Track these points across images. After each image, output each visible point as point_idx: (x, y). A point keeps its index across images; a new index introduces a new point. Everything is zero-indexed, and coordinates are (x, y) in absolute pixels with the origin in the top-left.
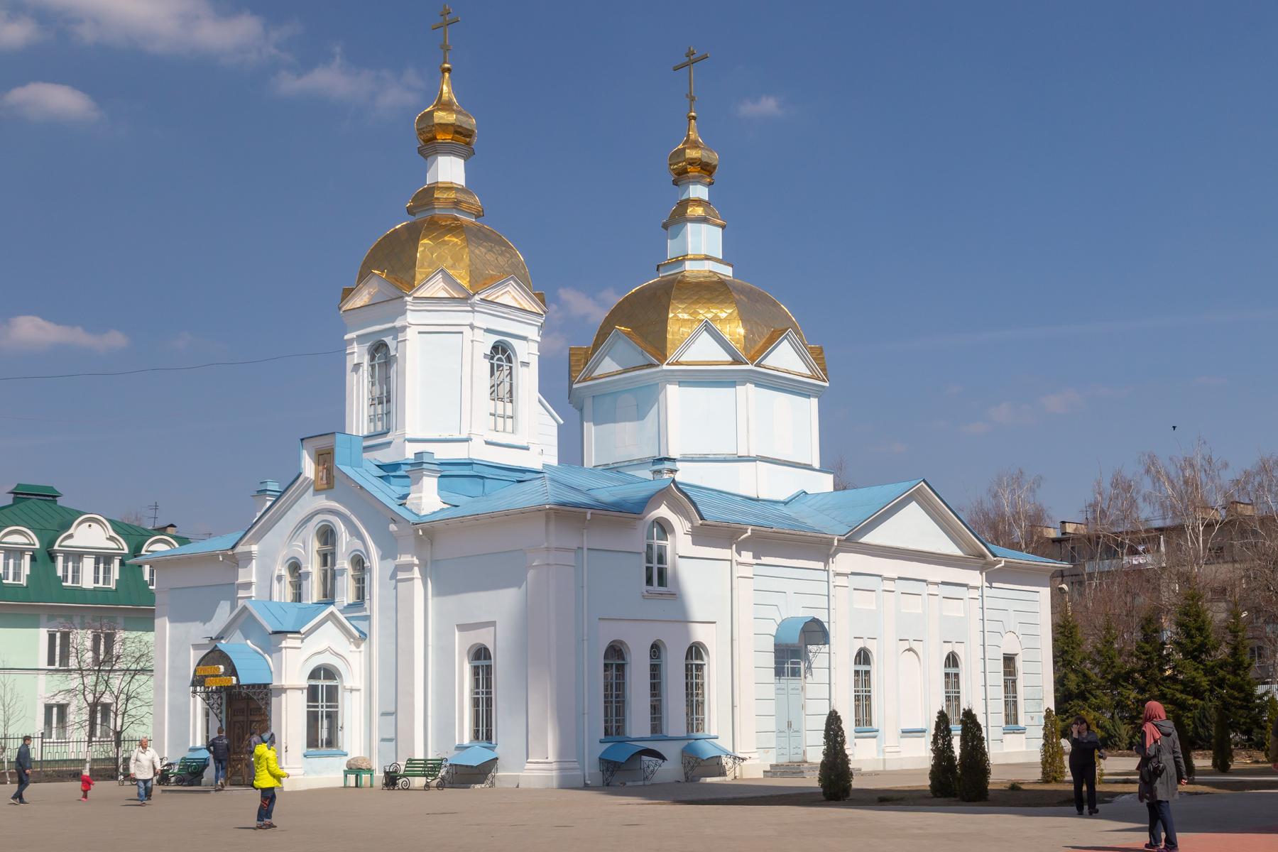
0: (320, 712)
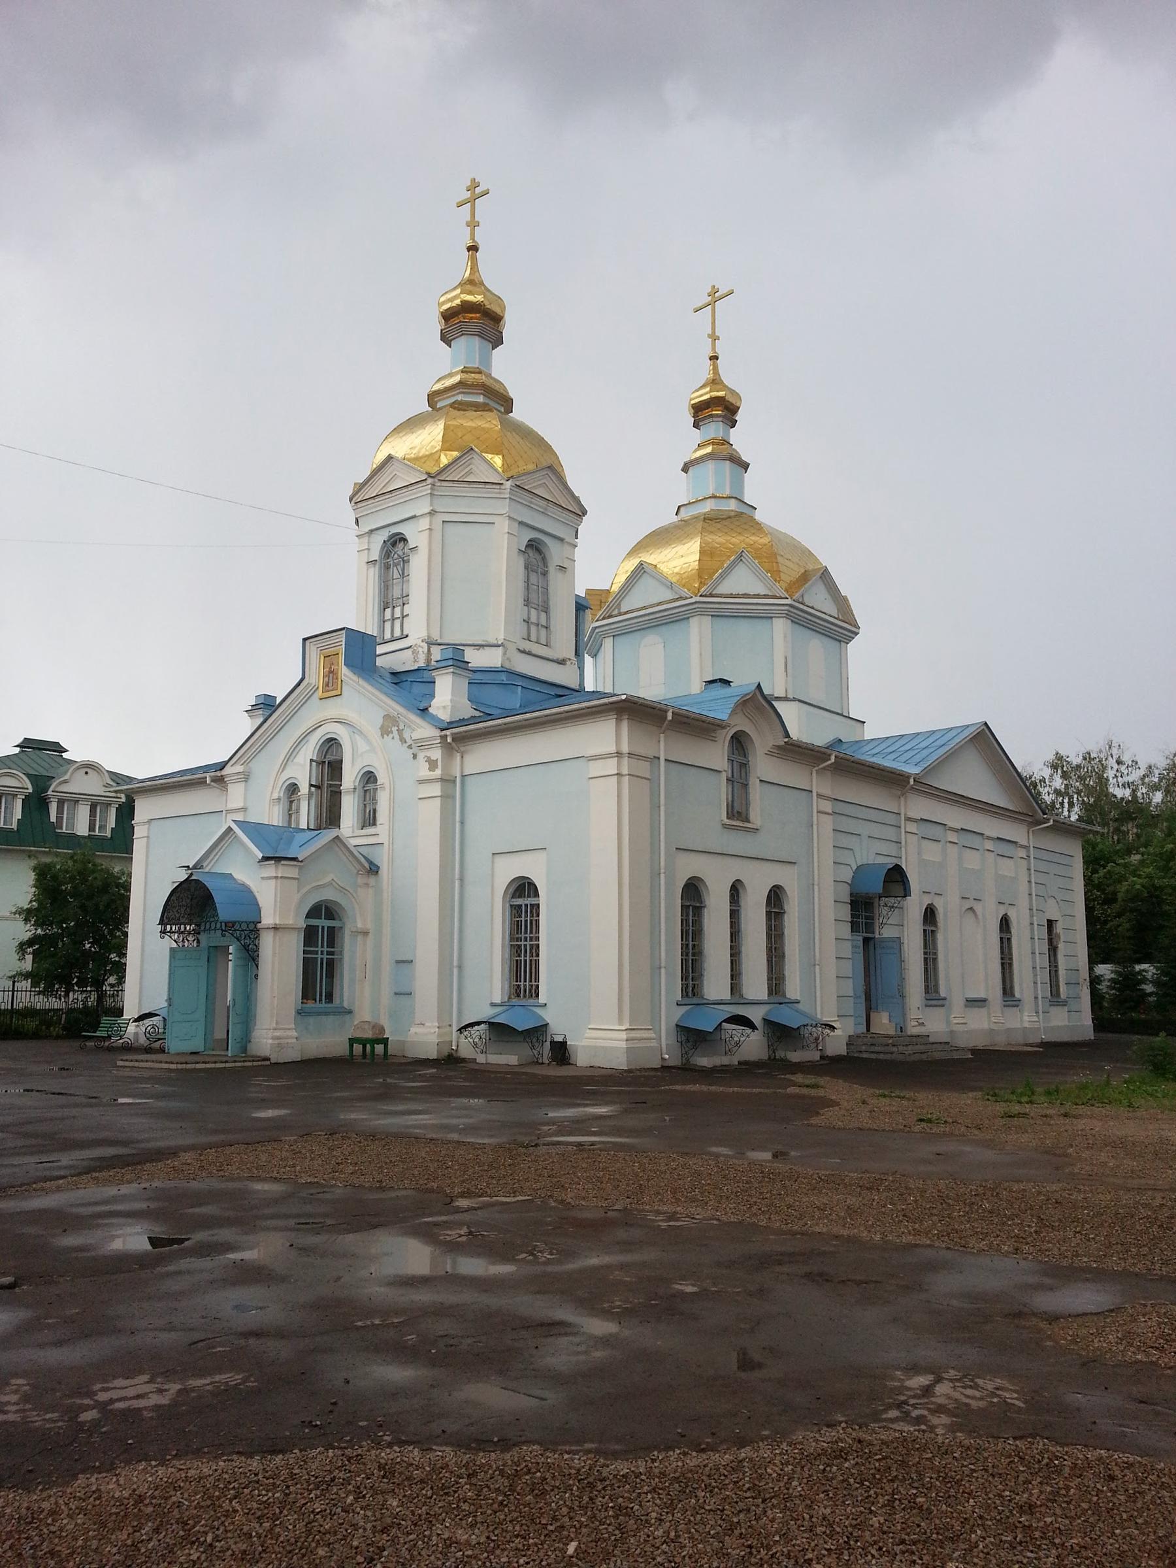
0: (328, 957)
